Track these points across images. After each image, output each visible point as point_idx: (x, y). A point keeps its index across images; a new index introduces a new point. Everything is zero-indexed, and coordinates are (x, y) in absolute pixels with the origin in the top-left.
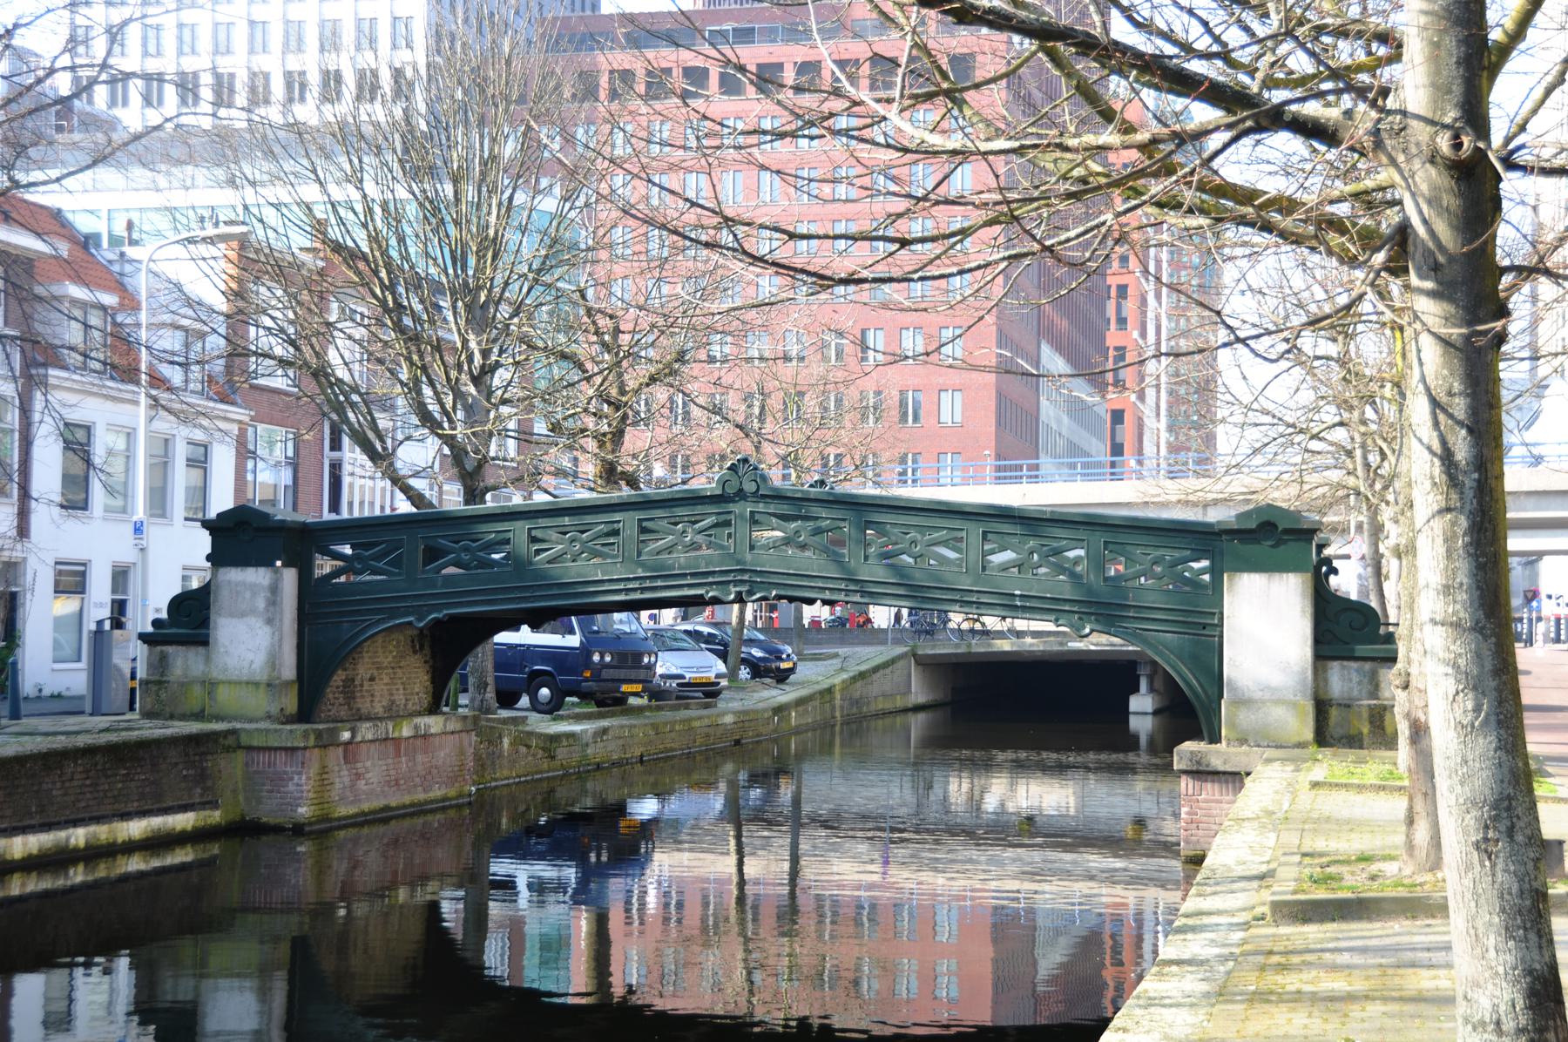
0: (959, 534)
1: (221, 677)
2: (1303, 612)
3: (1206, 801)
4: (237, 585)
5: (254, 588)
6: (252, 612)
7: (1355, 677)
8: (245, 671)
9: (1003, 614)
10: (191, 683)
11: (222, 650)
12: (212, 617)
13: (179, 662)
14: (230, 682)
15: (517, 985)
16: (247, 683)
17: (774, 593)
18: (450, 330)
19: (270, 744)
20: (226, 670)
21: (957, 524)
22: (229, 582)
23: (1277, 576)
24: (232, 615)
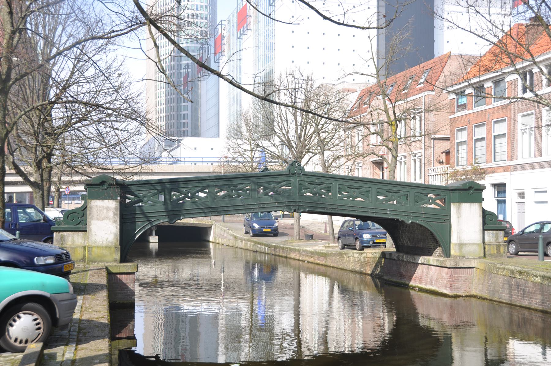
0: (369, 189)
1: (93, 245)
2: (480, 215)
3: (457, 277)
4: (100, 207)
5: (108, 209)
6: (107, 218)
7: (491, 235)
8: (104, 242)
9: (244, 212)
10: (77, 247)
11: (93, 234)
12: (88, 220)
13: (70, 239)
14: (98, 247)
15: (185, 361)
16: (106, 247)
17: (307, 210)
18: (42, 102)
19: (121, 272)
20: (96, 242)
21: (368, 186)
22: (96, 206)
23: (472, 204)
24: (98, 219)
